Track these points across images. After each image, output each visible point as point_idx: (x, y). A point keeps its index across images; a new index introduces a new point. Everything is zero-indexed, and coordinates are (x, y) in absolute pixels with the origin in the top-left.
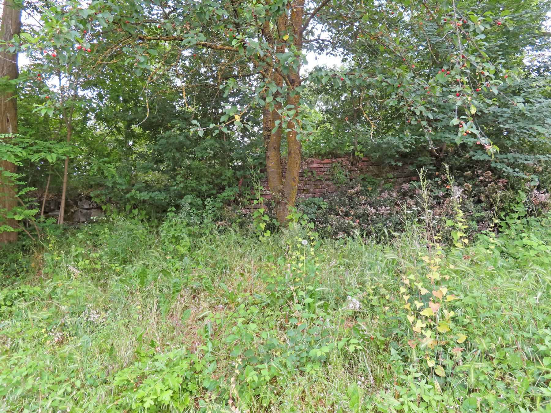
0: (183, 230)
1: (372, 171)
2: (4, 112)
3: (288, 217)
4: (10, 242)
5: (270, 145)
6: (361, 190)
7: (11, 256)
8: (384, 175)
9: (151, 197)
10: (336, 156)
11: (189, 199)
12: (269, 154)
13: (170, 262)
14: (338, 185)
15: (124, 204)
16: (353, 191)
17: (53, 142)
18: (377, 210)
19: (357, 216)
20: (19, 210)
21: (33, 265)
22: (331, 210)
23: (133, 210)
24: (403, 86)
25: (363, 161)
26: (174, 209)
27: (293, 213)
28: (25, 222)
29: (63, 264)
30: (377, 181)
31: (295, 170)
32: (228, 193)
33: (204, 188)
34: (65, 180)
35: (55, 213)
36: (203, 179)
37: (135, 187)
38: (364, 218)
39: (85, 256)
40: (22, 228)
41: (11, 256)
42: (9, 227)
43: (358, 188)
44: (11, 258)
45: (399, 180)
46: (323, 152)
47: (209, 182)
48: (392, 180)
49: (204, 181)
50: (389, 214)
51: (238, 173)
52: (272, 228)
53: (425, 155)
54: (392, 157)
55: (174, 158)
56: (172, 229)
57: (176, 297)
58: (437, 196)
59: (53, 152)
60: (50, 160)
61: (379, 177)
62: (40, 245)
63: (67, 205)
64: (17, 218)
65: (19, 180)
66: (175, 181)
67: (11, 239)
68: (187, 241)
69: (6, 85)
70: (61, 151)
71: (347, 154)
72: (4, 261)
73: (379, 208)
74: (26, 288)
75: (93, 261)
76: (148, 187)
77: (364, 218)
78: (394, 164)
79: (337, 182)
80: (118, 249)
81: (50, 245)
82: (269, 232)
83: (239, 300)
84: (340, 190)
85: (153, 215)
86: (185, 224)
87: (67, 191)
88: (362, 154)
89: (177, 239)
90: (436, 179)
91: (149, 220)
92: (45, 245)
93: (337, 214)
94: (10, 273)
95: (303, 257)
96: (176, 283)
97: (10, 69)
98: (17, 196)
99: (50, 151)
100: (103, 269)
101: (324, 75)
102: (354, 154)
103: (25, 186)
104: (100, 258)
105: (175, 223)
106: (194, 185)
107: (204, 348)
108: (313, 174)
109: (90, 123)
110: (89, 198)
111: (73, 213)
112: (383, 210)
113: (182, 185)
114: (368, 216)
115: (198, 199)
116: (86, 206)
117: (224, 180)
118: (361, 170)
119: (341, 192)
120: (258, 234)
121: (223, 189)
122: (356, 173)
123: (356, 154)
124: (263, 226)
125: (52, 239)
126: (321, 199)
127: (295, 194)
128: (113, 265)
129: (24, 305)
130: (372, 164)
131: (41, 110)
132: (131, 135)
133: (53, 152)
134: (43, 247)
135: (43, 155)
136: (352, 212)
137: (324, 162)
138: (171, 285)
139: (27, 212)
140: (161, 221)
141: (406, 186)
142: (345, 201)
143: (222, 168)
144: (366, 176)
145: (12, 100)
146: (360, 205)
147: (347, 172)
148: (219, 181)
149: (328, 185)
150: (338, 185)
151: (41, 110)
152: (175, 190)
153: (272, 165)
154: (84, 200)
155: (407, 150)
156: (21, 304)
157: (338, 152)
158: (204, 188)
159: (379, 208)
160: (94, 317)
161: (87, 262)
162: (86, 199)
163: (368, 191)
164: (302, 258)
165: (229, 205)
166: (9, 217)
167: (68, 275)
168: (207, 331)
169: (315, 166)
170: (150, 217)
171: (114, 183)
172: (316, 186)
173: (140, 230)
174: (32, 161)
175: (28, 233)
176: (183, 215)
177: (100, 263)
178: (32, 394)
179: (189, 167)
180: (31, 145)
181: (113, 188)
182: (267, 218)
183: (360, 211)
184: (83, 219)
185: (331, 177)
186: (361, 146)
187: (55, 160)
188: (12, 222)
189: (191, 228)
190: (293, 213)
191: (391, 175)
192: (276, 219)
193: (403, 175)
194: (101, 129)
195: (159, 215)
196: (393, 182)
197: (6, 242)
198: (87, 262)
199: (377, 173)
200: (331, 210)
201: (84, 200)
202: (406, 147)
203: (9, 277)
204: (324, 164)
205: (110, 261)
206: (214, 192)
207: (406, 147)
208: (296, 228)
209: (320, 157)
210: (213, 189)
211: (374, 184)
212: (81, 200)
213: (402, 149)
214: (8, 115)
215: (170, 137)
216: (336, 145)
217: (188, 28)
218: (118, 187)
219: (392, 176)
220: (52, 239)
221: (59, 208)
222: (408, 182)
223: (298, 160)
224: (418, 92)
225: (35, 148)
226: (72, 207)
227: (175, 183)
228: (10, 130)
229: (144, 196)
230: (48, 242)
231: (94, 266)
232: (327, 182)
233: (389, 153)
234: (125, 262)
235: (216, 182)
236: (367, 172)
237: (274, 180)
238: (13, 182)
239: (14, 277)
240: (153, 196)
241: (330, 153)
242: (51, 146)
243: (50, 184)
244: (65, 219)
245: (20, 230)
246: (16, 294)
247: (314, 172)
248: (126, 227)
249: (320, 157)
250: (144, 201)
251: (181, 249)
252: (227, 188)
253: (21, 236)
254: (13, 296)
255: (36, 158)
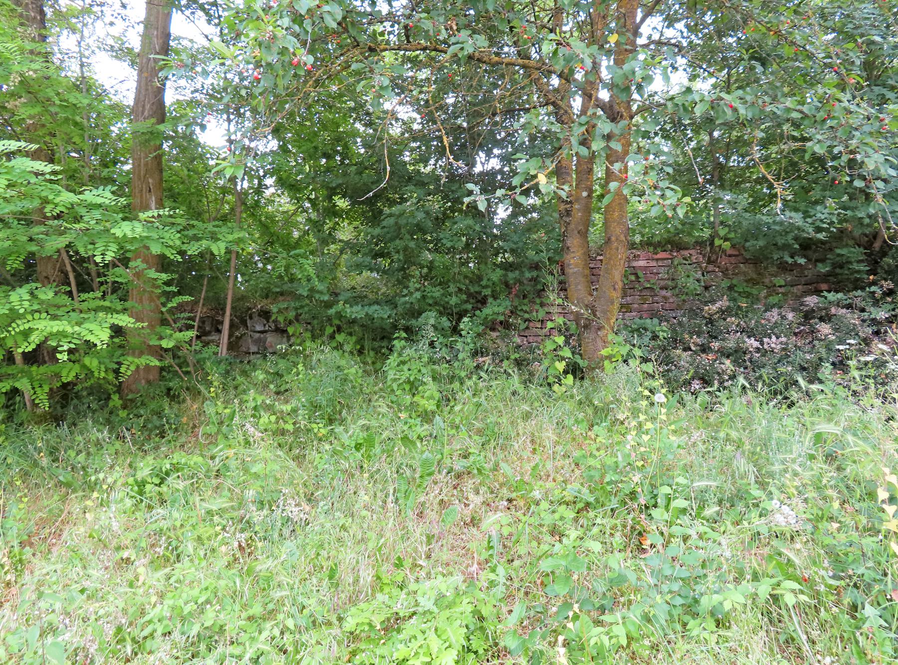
0: (424, 370)
1: (745, 274)
2: (144, 177)
3: (604, 352)
4: (149, 382)
5: (572, 226)
6: (729, 307)
7: (153, 405)
8: (767, 281)
9: (367, 314)
10: (679, 246)
11: (430, 318)
12: (569, 243)
13: (406, 423)
14: (684, 297)
15: (323, 323)
16: (714, 308)
17: (217, 223)
18: (762, 344)
19: (725, 353)
20: (168, 332)
21: (184, 420)
22: (675, 341)
23: (337, 336)
24: (834, 118)
25: (730, 256)
26: (404, 335)
27: (613, 345)
28: (174, 352)
29: (237, 420)
30: (755, 292)
31: (615, 274)
32: (493, 309)
33: (454, 300)
34: (231, 285)
35: (210, 338)
36: (452, 285)
37: (340, 298)
38: (737, 354)
39: (269, 408)
40: (168, 361)
41: (153, 405)
42: (152, 359)
43: (723, 303)
44: (152, 407)
45: (795, 290)
46: (657, 239)
47: (460, 290)
48: (781, 290)
49: (452, 289)
50: (784, 349)
51: (511, 275)
52: (574, 370)
53: (847, 245)
54: (786, 247)
55: (406, 249)
56: (405, 368)
57: (426, 483)
58: (874, 320)
59: (219, 239)
60: (216, 252)
61: (758, 283)
62: (195, 388)
63: (232, 326)
64: (165, 344)
65: (168, 283)
66: (407, 287)
67: (151, 377)
68: (431, 388)
69: (151, 133)
70: (230, 238)
71: (700, 243)
72: (142, 412)
73: (765, 340)
74: (179, 457)
75: (281, 417)
76: (358, 299)
77: (737, 354)
78: (790, 260)
79: (681, 292)
80: (322, 400)
81: (212, 389)
82: (570, 377)
83: (537, 494)
84: (687, 306)
85: (367, 344)
86: (425, 359)
87: (233, 302)
88: (728, 243)
89: (413, 387)
90: (873, 288)
91: (360, 352)
92: (202, 388)
93: (687, 349)
94: (151, 431)
95: (651, 427)
96: (427, 460)
97: (154, 108)
98: (164, 309)
99: (214, 238)
100: (297, 431)
101: (697, 100)
102: (712, 244)
103: (175, 294)
104: (295, 411)
105: (407, 361)
106: (437, 294)
107: (492, 576)
108: (637, 277)
109: (268, 193)
110: (265, 314)
111: (238, 338)
112: (772, 343)
113: (418, 295)
114: (745, 353)
115: (445, 319)
116: (259, 328)
117: (486, 287)
118: (725, 272)
119: (691, 310)
120: (551, 380)
121: (483, 302)
122: (716, 276)
123: (717, 242)
124: (561, 366)
125: (215, 379)
126: (656, 321)
127: (616, 312)
128: (314, 426)
129: (181, 485)
130: (746, 261)
131: (225, 168)
132: (333, 212)
133: (219, 239)
134: (199, 393)
135: (204, 243)
136: (715, 345)
137: (658, 256)
138: (416, 463)
139: (178, 335)
140: (382, 355)
141: (812, 301)
142: (700, 326)
143: (482, 266)
144: (735, 282)
145: (156, 157)
146: (728, 333)
147: (699, 275)
148: (477, 289)
149: (665, 298)
150: (684, 297)
151: (225, 168)
152: (406, 303)
153: (574, 261)
154: (256, 318)
155: (821, 236)
156: (176, 483)
157: (686, 239)
158: (454, 300)
159: (765, 340)
160: (293, 511)
161: (273, 418)
162: (260, 315)
163: (739, 308)
164: (649, 425)
165: (493, 329)
166: (154, 342)
167: (245, 438)
168: (492, 547)
169: (642, 263)
170: (362, 348)
171: (312, 290)
172: (644, 300)
173: (353, 370)
174: (189, 253)
175: (177, 368)
176: (423, 345)
177: (291, 422)
178: (211, 637)
179: (431, 266)
180: (185, 229)
181: (310, 297)
182: (567, 353)
183: (731, 344)
184: (253, 349)
185: (670, 283)
186: (727, 229)
187: (223, 251)
188: (160, 352)
189: (436, 367)
190: (613, 345)
191: (779, 281)
192: (581, 355)
193: (803, 280)
194: (285, 203)
195: (376, 344)
196: (783, 294)
197: (143, 381)
198: (273, 418)
199: (755, 276)
200: (675, 341)
201: (256, 318)
202: (819, 230)
203: (149, 438)
204: (657, 260)
205: (309, 418)
206: (469, 307)
207: (819, 230)
208: (624, 373)
209: (651, 249)
210: (466, 302)
211: (748, 295)
212: (251, 318)
213: (810, 232)
214: (150, 181)
215: (401, 215)
216: (680, 227)
217: (455, 28)
218: (317, 296)
219: (783, 283)
220: (215, 379)
221: (219, 331)
222: (818, 292)
223: (622, 253)
224: (867, 128)
225: (191, 233)
226: (238, 329)
227: (405, 291)
228: (153, 205)
229: (356, 312)
230: (209, 384)
231: (282, 424)
232: (664, 292)
233: (780, 241)
234: (331, 421)
235: (472, 290)
236: (736, 274)
237: (578, 287)
238: (159, 287)
239: (157, 439)
240: (370, 313)
241: (669, 242)
242: (216, 229)
243: (206, 292)
244: (228, 349)
245: (166, 363)
246: (168, 466)
247: (640, 274)
248: (327, 364)
249: (651, 249)
250: (354, 322)
251: (423, 402)
252: (490, 300)
253: (164, 373)
254: (164, 470)
255: (194, 249)
